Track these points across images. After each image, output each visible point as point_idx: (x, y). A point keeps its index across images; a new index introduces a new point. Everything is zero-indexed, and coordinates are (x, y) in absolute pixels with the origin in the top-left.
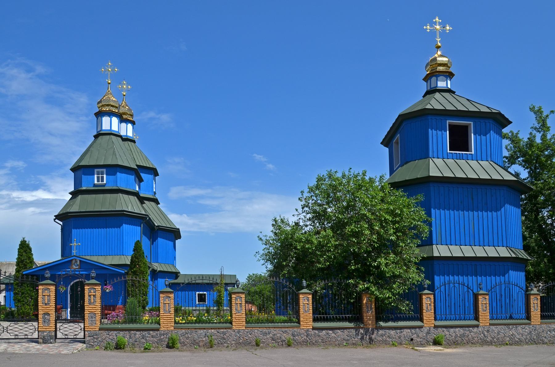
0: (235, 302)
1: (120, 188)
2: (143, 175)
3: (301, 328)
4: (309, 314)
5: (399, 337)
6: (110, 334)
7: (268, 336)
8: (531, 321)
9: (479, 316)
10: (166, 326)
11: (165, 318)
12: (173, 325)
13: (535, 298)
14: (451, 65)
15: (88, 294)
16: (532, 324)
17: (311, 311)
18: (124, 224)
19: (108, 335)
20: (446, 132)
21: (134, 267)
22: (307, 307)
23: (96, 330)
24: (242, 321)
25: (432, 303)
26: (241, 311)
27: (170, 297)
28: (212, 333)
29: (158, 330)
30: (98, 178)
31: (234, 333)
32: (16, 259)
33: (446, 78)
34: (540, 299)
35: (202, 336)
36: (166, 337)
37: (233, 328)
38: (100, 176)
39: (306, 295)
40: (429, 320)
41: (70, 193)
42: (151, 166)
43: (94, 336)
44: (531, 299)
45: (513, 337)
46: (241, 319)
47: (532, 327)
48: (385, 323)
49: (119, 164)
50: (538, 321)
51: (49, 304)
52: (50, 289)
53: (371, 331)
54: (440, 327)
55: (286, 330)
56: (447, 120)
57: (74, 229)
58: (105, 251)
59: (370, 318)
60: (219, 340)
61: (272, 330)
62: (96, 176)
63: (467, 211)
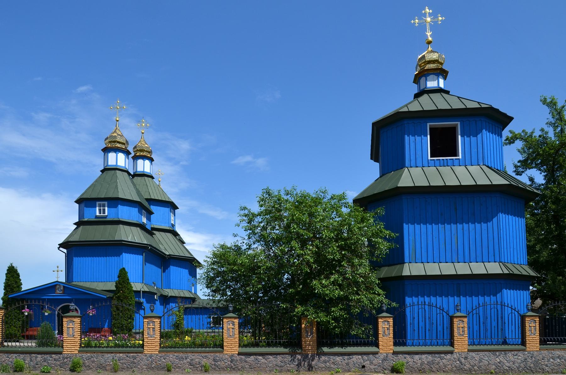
1: (121, 220)
3: (225, 353)
5: (347, 364)
7: (184, 360)
8: (526, 347)
9: (454, 341)
10: (70, 350)
11: (69, 341)
13: (532, 320)
14: (444, 61)
16: (527, 350)
17: (392, 335)
18: (123, 253)
19: (8, 357)
20: (426, 137)
21: (118, 293)
22: (232, 332)
25: (390, 327)
27: (74, 321)
28: (120, 357)
29: (61, 353)
30: (100, 210)
31: (146, 357)
33: (437, 77)
34: (538, 321)
36: (70, 360)
37: (145, 353)
38: (102, 208)
39: (231, 319)
40: (386, 345)
44: (526, 322)
45: (500, 365)
46: (154, 344)
47: (528, 353)
48: (330, 349)
49: (119, 197)
50: (536, 347)
53: (311, 357)
54: (401, 353)
55: (206, 355)
56: (427, 123)
58: (105, 278)
59: (309, 344)
60: (128, 365)
62: (97, 208)
63: (431, 224)
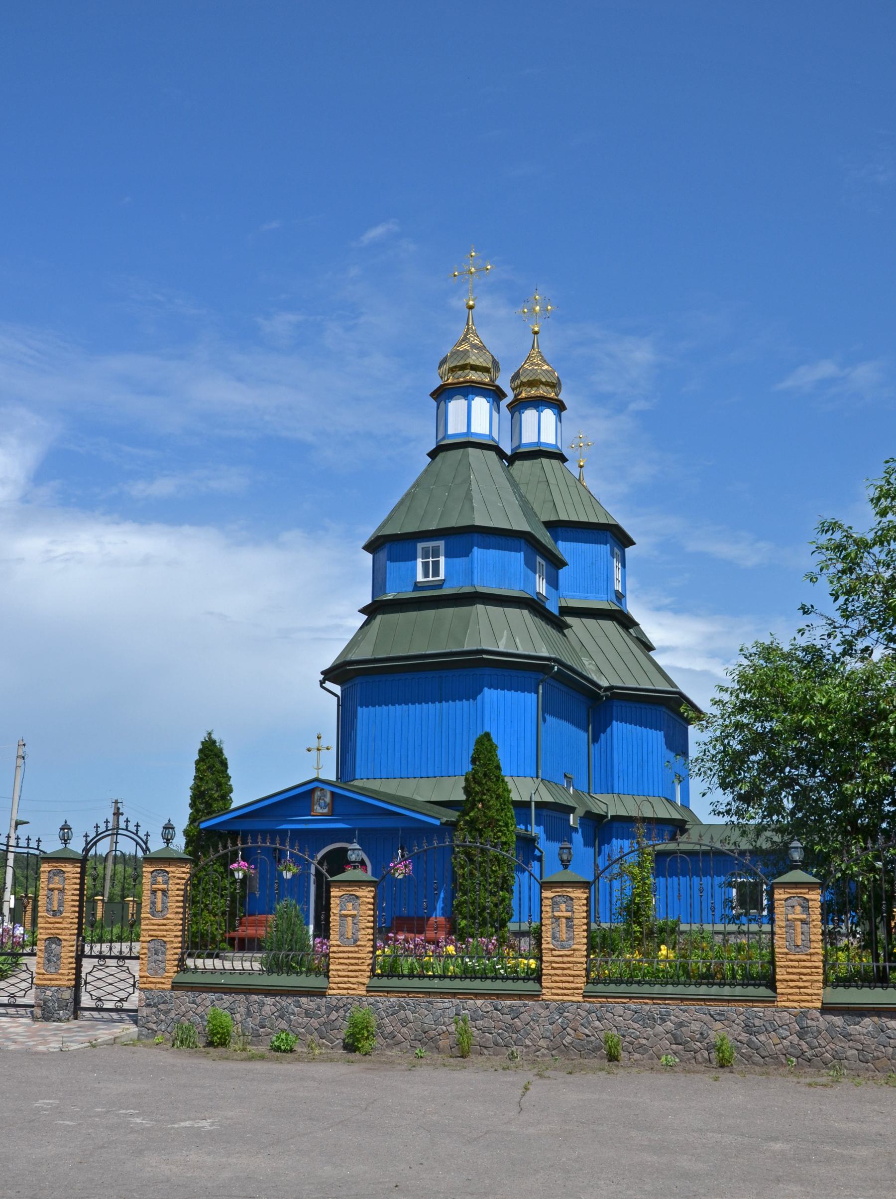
0: (550, 914)
2: (564, 549)
3: (780, 1004)
4: (809, 957)
6: (198, 1000)
10: (345, 983)
12: (366, 981)
15: (149, 887)
18: (486, 689)
19: (194, 1002)
21: (472, 809)
22: (802, 934)
23: (163, 989)
24: (574, 976)
26: (571, 942)
29: (320, 993)
30: (426, 565)
32: (191, 788)
35: (446, 1019)
36: (345, 1016)
38: (431, 559)
41: (363, 611)
42: (603, 520)
43: (159, 1006)
46: (569, 968)
49: (476, 524)
51: (61, 914)
52: (64, 872)
57: (362, 707)
61: (673, 1007)
62: (419, 561)
